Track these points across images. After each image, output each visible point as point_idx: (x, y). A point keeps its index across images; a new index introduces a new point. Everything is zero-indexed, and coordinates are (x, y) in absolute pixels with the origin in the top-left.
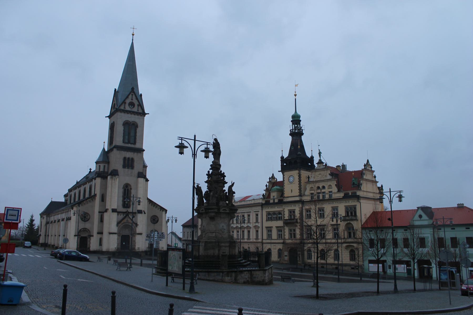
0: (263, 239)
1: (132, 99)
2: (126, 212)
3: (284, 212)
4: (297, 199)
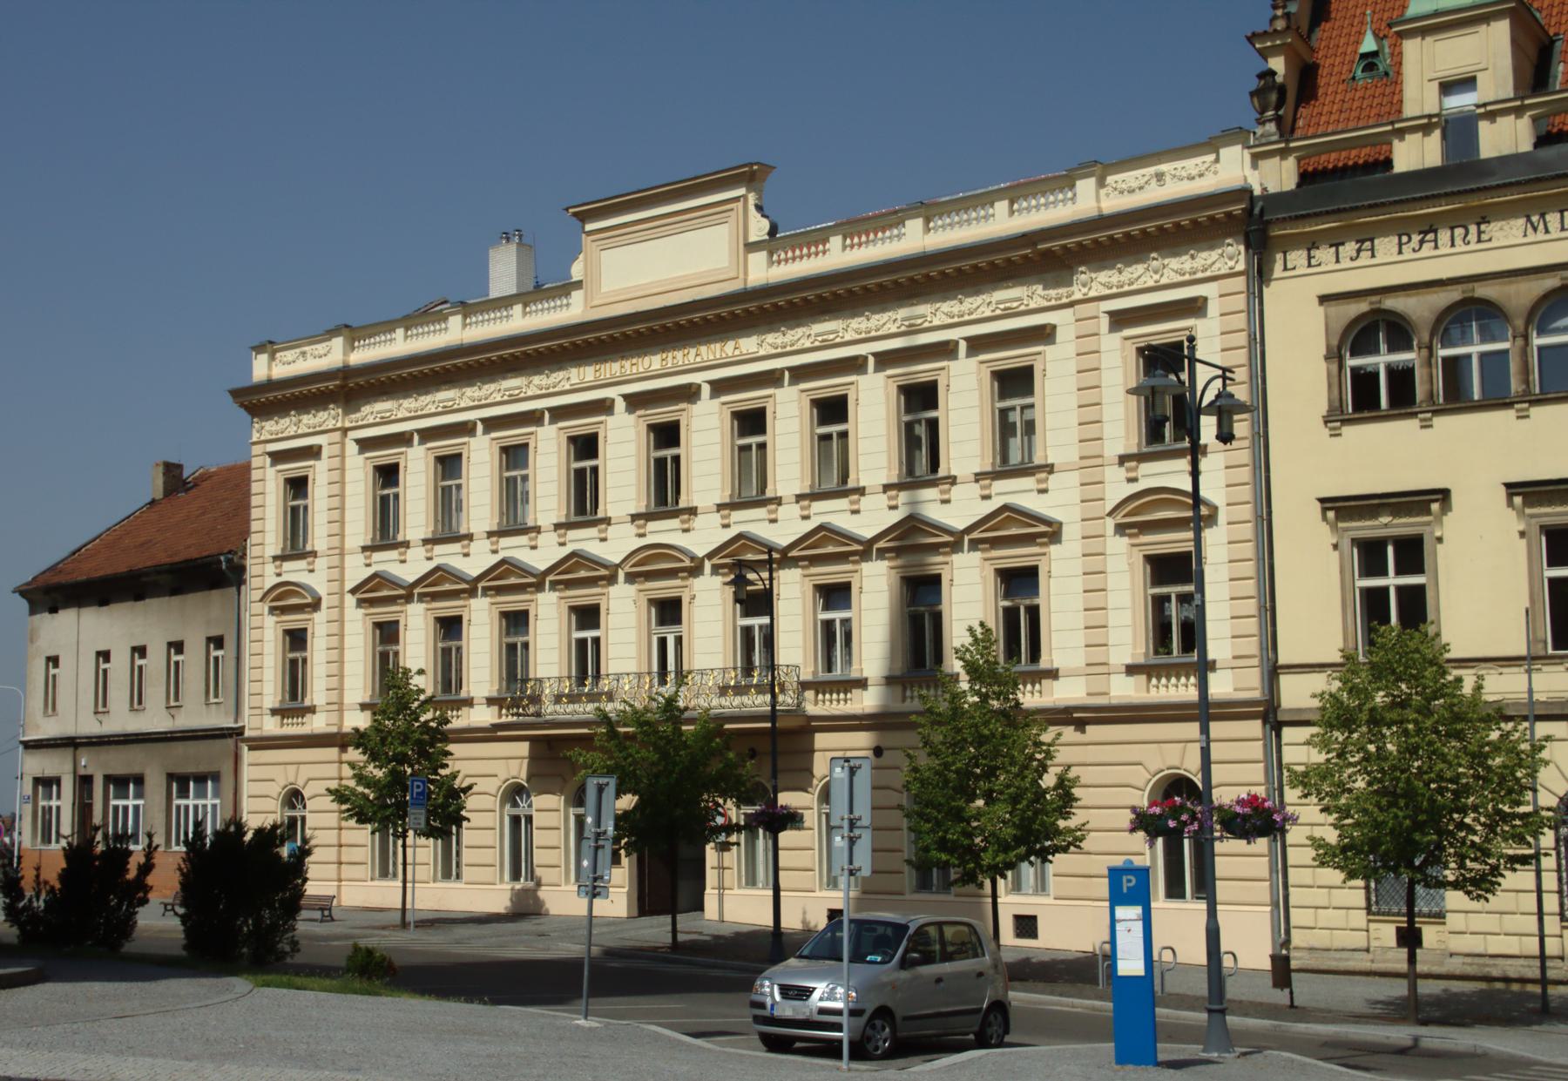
0: (1274, 672)
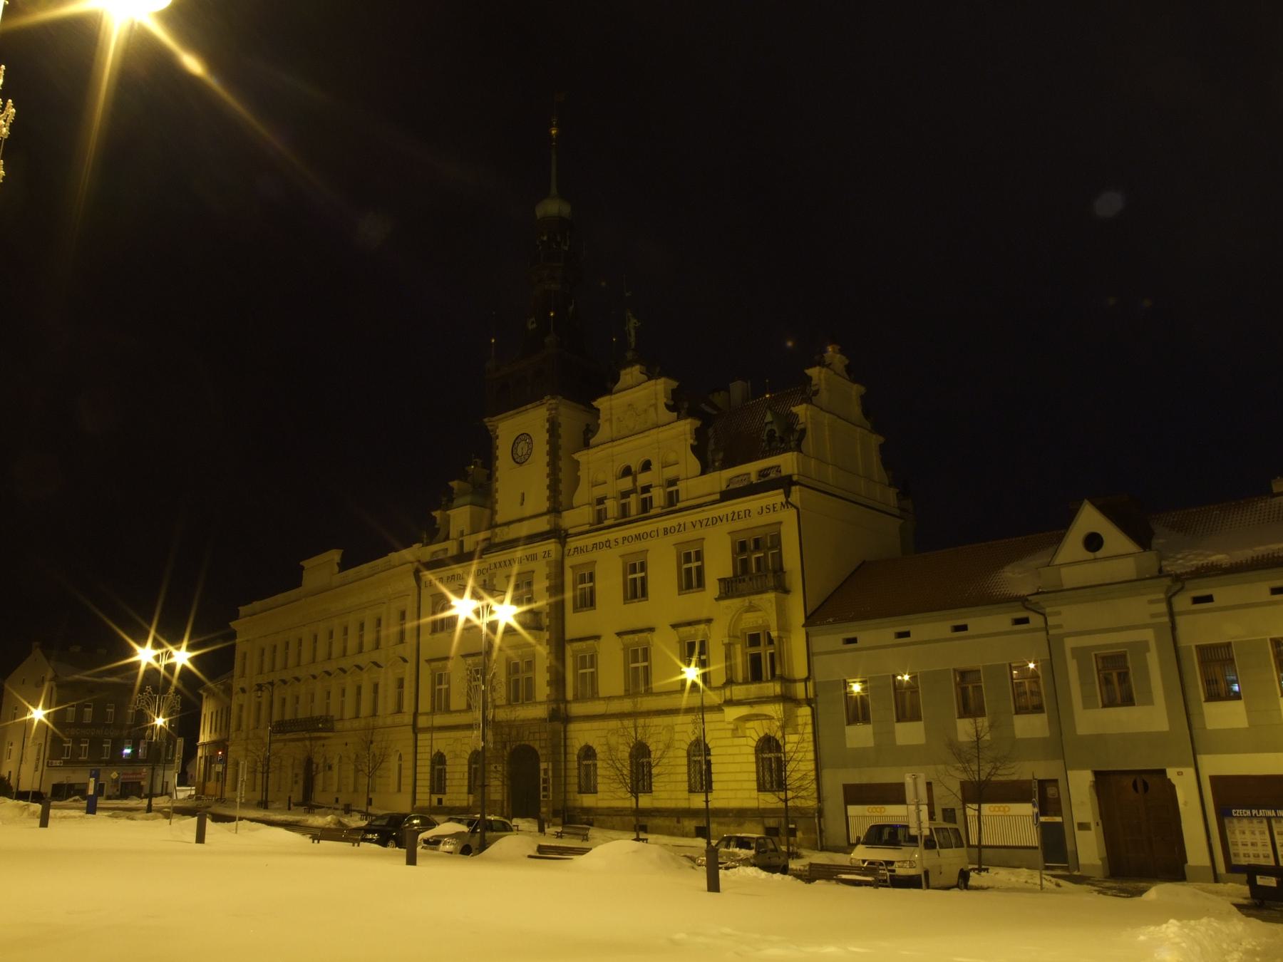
4: (543, 525)
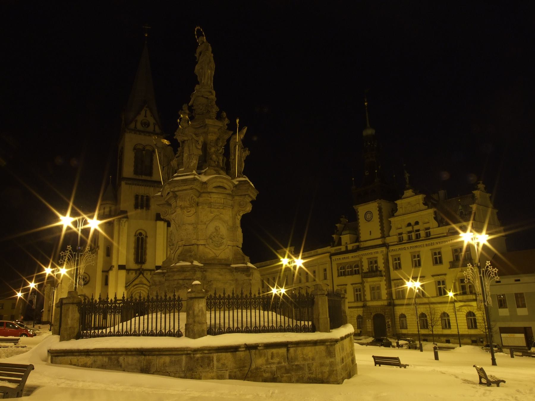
1: (146, 116)
2: (139, 269)
3: (362, 262)
4: (379, 242)
